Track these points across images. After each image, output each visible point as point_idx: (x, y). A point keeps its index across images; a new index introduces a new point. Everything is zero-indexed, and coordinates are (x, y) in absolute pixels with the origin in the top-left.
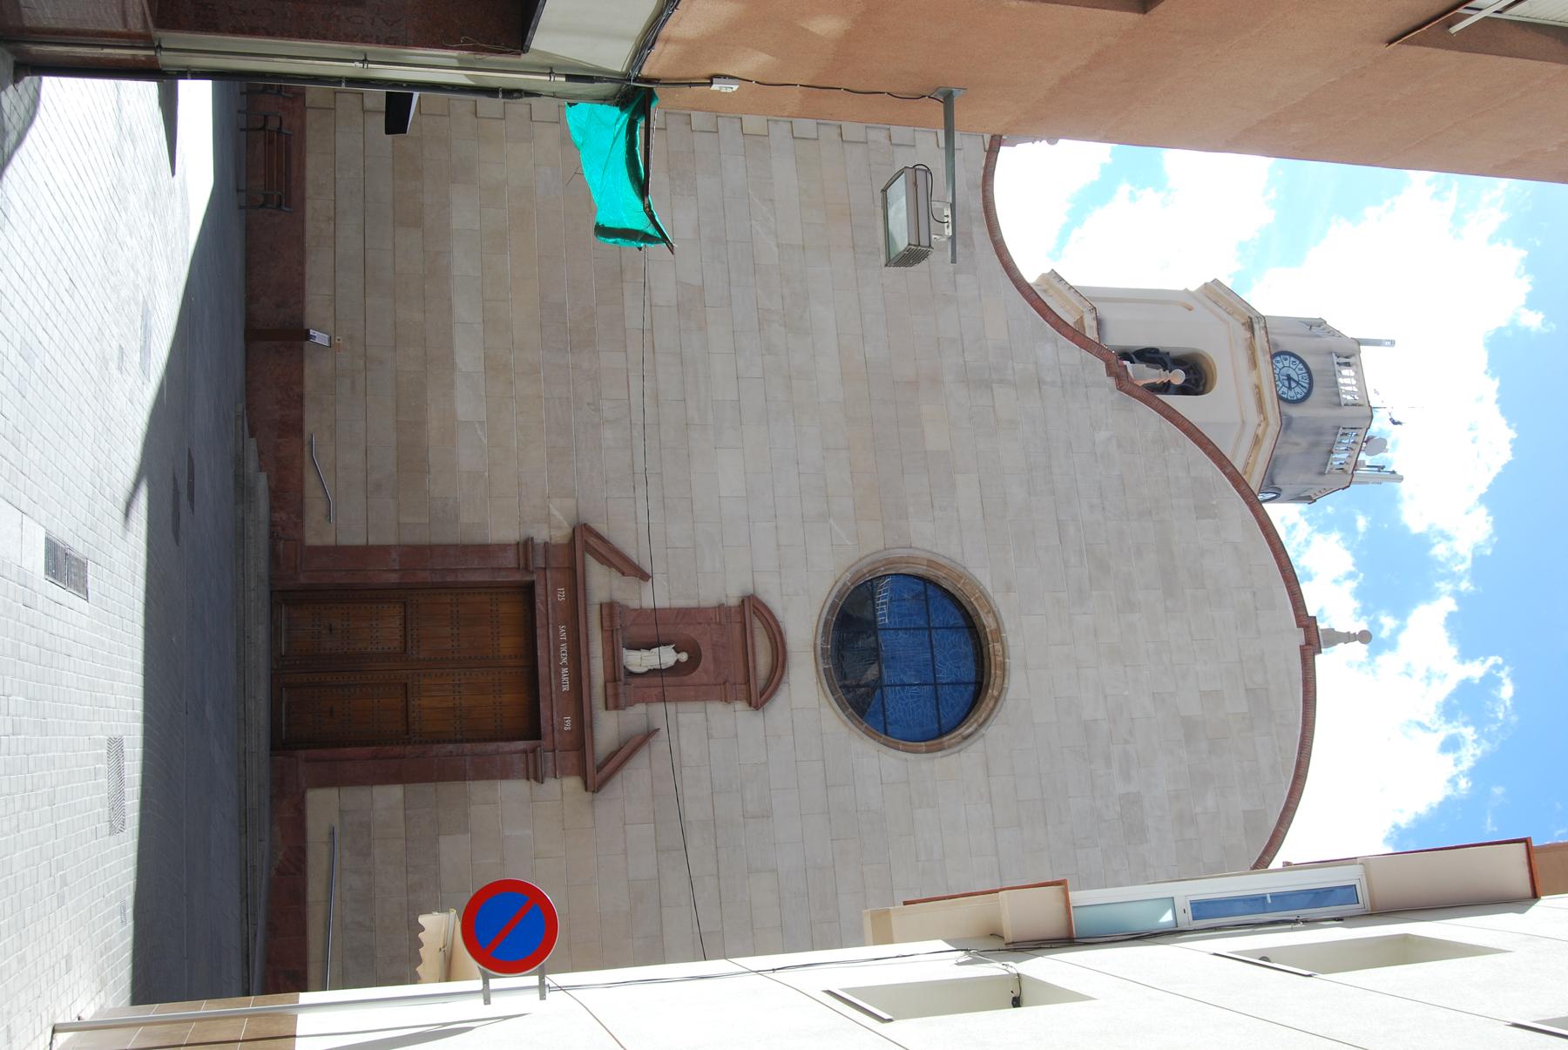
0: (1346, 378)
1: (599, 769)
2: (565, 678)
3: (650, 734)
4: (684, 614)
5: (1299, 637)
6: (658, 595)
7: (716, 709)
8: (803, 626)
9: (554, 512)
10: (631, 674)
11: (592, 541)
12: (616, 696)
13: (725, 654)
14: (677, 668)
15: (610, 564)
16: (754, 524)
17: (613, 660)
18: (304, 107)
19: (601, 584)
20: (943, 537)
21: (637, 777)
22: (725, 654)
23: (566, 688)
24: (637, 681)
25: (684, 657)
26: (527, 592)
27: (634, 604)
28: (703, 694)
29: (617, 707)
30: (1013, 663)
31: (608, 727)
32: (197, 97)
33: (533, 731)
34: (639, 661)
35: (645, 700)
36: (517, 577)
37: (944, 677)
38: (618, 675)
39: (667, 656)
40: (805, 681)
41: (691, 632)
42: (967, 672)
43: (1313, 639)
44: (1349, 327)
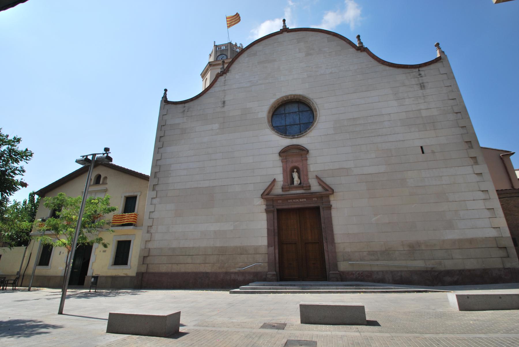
0: (223, 48)
1: (327, 190)
2: (302, 200)
3: (317, 177)
4: (284, 171)
5: (286, 34)
6: (280, 178)
7: (309, 162)
8: (286, 142)
9: (257, 204)
10: (300, 184)
11: (266, 193)
12: (306, 187)
13: (294, 158)
14: (298, 172)
15: (271, 189)
16: (260, 156)
17: (297, 188)
18: (146, 273)
19: (278, 190)
20: (263, 111)
21: (329, 181)
22: (294, 158)
23: (305, 200)
24: (302, 181)
25: (295, 170)
26: (279, 211)
27: (282, 183)
28: (306, 166)
29: (310, 186)
30: (294, 93)
31: (315, 187)
32: (68, 290)
33: (318, 208)
34: (296, 181)
35: (308, 179)
36: (276, 213)
37: (297, 110)
38: (300, 186)
39: (295, 175)
40: (302, 141)
41: (288, 170)
42: (294, 108)
43: (285, 30)
44: (212, 48)
